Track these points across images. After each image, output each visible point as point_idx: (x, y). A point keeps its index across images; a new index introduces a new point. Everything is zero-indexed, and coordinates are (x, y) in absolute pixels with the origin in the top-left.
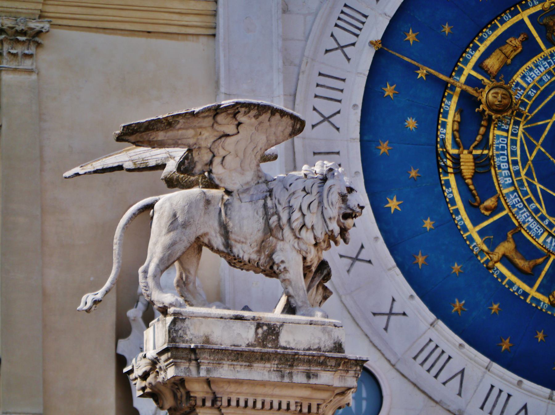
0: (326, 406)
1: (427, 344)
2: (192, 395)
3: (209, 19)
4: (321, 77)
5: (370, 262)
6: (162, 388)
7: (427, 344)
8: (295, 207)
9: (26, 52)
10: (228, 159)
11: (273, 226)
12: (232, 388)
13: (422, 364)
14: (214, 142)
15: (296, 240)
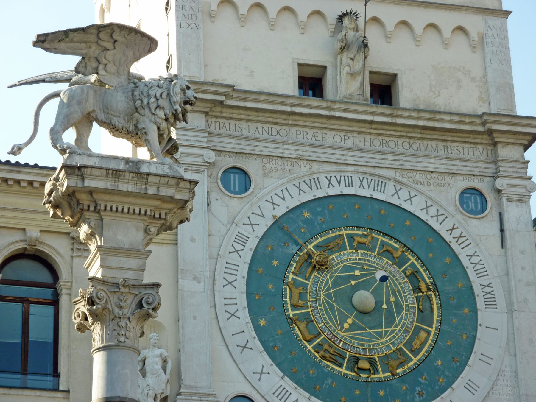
0: (172, 216)
1: (280, 387)
2: (81, 202)
3: (174, 236)
4: (227, 264)
5: (251, 349)
6: (62, 201)
7: (280, 387)
8: (152, 95)
9: (85, 248)
10: (109, 66)
11: (137, 106)
12: (107, 197)
13: (277, 397)
14: (99, 54)
15: (153, 116)
